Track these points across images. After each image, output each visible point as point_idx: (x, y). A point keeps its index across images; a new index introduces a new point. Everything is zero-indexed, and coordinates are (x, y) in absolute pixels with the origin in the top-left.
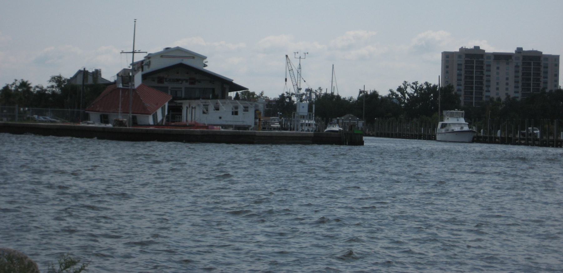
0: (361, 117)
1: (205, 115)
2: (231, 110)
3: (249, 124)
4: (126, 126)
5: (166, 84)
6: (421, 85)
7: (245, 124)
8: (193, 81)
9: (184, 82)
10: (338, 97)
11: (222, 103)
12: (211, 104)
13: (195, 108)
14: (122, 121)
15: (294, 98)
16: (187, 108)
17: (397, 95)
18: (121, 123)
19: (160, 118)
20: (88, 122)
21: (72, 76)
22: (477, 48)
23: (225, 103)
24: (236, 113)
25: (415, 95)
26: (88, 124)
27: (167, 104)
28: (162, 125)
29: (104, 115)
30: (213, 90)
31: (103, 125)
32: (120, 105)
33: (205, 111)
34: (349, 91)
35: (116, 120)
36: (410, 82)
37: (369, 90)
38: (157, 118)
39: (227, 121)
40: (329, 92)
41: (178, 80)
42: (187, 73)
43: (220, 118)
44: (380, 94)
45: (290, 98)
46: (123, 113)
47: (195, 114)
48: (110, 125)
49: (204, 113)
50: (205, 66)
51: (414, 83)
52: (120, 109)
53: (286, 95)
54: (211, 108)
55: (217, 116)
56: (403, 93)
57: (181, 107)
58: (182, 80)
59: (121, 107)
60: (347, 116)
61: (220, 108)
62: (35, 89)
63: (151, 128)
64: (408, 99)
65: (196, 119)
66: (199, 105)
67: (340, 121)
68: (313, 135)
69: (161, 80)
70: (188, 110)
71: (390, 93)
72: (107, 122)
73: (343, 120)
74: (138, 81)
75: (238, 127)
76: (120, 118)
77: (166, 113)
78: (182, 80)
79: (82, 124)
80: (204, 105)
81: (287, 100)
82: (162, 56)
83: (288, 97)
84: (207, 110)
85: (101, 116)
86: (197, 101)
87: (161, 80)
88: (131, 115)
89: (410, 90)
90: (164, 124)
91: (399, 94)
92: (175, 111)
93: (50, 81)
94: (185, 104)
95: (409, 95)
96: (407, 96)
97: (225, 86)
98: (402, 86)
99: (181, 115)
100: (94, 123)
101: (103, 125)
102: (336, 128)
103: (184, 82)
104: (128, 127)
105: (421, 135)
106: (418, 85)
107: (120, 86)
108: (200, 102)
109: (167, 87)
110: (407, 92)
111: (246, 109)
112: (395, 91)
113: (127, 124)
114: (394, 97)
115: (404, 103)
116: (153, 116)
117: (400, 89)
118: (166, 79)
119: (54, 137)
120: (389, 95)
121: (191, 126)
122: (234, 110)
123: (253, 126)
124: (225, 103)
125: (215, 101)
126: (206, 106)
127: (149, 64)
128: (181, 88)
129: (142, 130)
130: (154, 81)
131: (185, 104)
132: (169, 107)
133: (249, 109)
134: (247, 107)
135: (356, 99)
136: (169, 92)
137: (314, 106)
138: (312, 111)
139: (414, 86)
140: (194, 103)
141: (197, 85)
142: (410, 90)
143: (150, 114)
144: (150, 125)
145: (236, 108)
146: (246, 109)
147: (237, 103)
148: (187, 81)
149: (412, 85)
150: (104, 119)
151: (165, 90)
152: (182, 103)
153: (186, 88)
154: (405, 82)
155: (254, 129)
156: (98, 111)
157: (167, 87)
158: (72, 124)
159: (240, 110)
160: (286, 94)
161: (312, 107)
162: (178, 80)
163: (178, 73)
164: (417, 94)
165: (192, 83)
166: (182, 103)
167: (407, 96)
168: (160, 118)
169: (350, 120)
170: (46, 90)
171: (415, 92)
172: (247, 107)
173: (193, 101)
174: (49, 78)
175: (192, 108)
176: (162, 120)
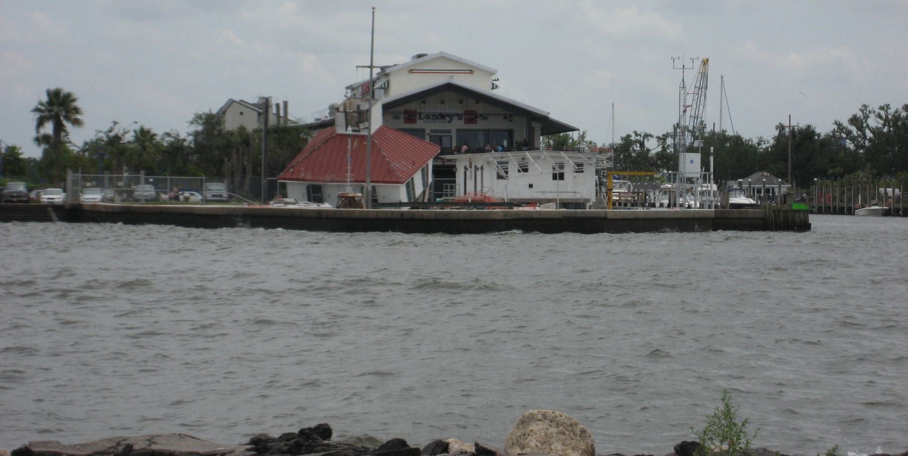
0: (783, 175)
1: (501, 181)
2: (551, 171)
3: (585, 196)
4: (362, 208)
5: (420, 124)
6: (896, 112)
7: (578, 196)
8: (471, 117)
9: (455, 118)
10: (737, 139)
11: (533, 158)
12: (513, 159)
13: (482, 168)
14: (353, 198)
15: (570, 141)
16: (465, 168)
17: (849, 133)
18: (351, 202)
19: (419, 189)
20: (286, 200)
21: (309, 120)
22: (326, 424)
23: (539, 157)
24: (561, 177)
25: (886, 130)
26: (286, 203)
27: (430, 163)
28: (423, 203)
29: (313, 186)
30: (510, 133)
31: (314, 206)
32: (349, 168)
33: (503, 173)
34: (758, 129)
35: (340, 197)
36: (874, 106)
37: (800, 122)
38: (413, 189)
39: (543, 192)
40: (717, 130)
41: (442, 116)
42: (461, 102)
43: (531, 186)
44: (817, 131)
45: (642, 144)
46: (355, 181)
47: (487, 179)
48: (326, 206)
49: (500, 177)
50: (494, 87)
51: (882, 108)
52: (349, 175)
53: (633, 138)
54: (513, 168)
55: (531, 181)
56: (860, 128)
57: (455, 166)
58: (451, 116)
59: (352, 172)
60: (758, 175)
61: (530, 168)
62: (163, 139)
63: (406, 209)
64: (870, 140)
65: (485, 190)
66: (489, 163)
67: (745, 186)
68: (713, 216)
69: (410, 117)
70: (468, 174)
71: (836, 127)
72: (320, 200)
73: (750, 183)
74: (377, 120)
75: (565, 204)
76: (350, 191)
77: (430, 180)
78: (451, 116)
79: (274, 205)
80: (499, 163)
81: (637, 148)
82: (411, 71)
83: (636, 141)
84: (507, 173)
85: (308, 188)
86: (486, 156)
87: (410, 117)
88: (368, 186)
89: (873, 122)
90: (426, 200)
91: (854, 129)
92: (445, 174)
93: (192, 123)
94: (461, 162)
95: (872, 131)
96: (869, 134)
97: (534, 124)
98: (859, 114)
99: (455, 182)
100: (296, 201)
101: (314, 206)
102: (742, 200)
103: (455, 118)
104: (365, 209)
105: (829, 208)
106: (889, 111)
107: (340, 130)
108: (492, 157)
109: (423, 131)
110: (868, 125)
111: (579, 168)
112: (845, 123)
113: (363, 202)
114: (844, 135)
115: (863, 147)
116: (408, 186)
117: (854, 120)
118: (420, 114)
119: (298, 232)
120: (834, 131)
121: (475, 204)
122: (558, 171)
123: (593, 199)
124: (539, 157)
125: (520, 154)
126: (503, 164)
127: (386, 88)
128: (450, 131)
129: (392, 213)
130: (396, 118)
131: (461, 162)
132: (434, 167)
133: (585, 168)
134: (582, 165)
135: (772, 142)
136: (427, 138)
137: (712, 159)
138: (708, 170)
139: (883, 113)
140: (479, 159)
141: (480, 125)
142: (873, 122)
143: (402, 183)
144: (401, 204)
145: (561, 166)
146: (579, 168)
147: (561, 157)
148: (460, 117)
149: (877, 111)
150: (315, 194)
151: (419, 133)
152: (455, 160)
153: (458, 130)
154: (865, 106)
155: (594, 205)
156: (303, 180)
157: (423, 131)
158: (257, 206)
159: (568, 172)
160: (633, 135)
161: (709, 162)
162: (442, 116)
163: (442, 102)
164: (890, 127)
165: (468, 121)
166: (455, 160)
167: (869, 134)
168: (419, 189)
169: (764, 183)
170: (184, 140)
171: (884, 125)
172: (582, 165)
173: (478, 155)
174: (191, 117)
175: (476, 168)
176: (424, 192)
